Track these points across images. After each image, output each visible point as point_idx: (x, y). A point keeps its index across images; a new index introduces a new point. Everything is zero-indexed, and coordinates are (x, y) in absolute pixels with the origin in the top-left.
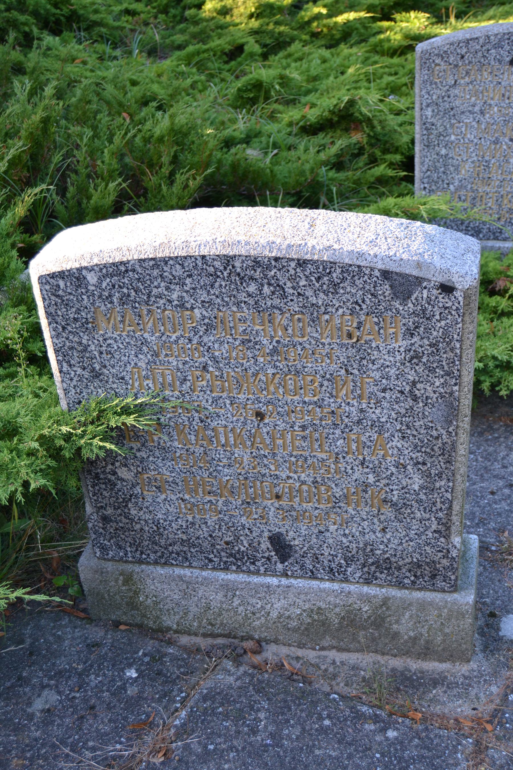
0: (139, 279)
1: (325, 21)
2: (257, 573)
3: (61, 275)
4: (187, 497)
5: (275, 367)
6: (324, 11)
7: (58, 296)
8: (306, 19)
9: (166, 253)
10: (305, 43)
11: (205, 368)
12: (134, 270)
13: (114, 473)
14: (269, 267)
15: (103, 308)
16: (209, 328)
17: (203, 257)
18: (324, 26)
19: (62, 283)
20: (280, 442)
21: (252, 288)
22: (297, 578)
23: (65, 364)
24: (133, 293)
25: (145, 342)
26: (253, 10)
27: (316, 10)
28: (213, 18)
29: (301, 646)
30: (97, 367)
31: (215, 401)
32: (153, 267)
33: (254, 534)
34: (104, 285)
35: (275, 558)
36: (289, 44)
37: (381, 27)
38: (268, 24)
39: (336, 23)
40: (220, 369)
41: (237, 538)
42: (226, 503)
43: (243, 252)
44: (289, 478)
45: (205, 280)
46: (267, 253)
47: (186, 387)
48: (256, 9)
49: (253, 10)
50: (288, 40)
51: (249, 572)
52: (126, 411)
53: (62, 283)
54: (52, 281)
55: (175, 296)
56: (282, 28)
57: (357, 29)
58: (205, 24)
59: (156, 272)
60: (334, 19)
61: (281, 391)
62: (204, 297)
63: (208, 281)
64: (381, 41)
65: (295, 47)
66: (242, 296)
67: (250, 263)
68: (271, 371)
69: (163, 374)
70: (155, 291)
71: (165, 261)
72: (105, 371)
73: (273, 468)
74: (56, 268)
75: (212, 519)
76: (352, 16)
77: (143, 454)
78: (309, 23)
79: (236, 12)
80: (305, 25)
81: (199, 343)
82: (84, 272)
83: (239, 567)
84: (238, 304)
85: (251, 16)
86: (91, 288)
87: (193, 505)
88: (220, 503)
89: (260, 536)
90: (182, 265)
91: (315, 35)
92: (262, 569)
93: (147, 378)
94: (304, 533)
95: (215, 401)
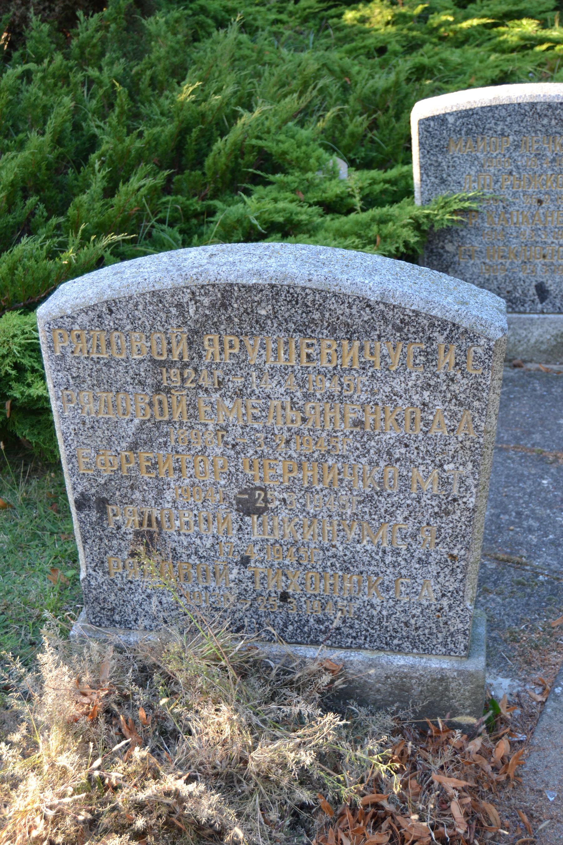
0: (479, 119)
1: (453, 27)
2: (524, 312)
3: (433, 118)
4: (487, 261)
5: (553, 170)
6: (451, 19)
7: (428, 132)
8: (435, 25)
9: (497, 103)
10: (435, 45)
11: (511, 173)
12: (477, 114)
13: (443, 248)
14: (556, 109)
15: (455, 138)
16: (517, 147)
17: (519, 104)
18: (451, 31)
19: (432, 124)
20: (549, 219)
21: (545, 121)
22: (549, 313)
23: (425, 176)
24: (474, 128)
25: (477, 158)
26: (390, 18)
27: (443, 18)
28: (353, 26)
29: (548, 362)
30: (445, 176)
31: (514, 194)
32: (489, 111)
33: (527, 284)
34: (458, 123)
35: (537, 300)
36: (420, 46)
37: (498, 32)
38: (402, 30)
39: (461, 28)
40: (519, 173)
41: (515, 288)
42: (512, 263)
43: (542, 100)
44: (553, 243)
45: (518, 118)
46: (556, 101)
47: (497, 186)
48: (393, 17)
49: (390, 18)
50: (419, 42)
51: (520, 312)
52: (462, 200)
53: (432, 124)
54: (426, 122)
55: (499, 128)
56: (415, 33)
57: (473, 35)
58: (348, 30)
59: (490, 114)
60: (459, 25)
61: (554, 185)
62: (516, 128)
63: (518, 118)
64: (500, 42)
65: (427, 47)
66: (539, 127)
67: (546, 106)
68: (550, 173)
69: (484, 179)
70: (488, 126)
71: (496, 107)
72: (449, 179)
73: (543, 236)
74: (429, 114)
75: (500, 275)
76: (475, 22)
77: (464, 233)
78: (437, 29)
79: (373, 20)
80: (433, 31)
81: (510, 158)
82: (447, 116)
83: (513, 309)
84: (535, 132)
85: (388, 23)
86: (450, 126)
87: (491, 266)
88: (507, 264)
89: (530, 285)
90: (506, 110)
91: (442, 39)
92: (528, 309)
93: (474, 181)
94: (557, 280)
95: (514, 194)
